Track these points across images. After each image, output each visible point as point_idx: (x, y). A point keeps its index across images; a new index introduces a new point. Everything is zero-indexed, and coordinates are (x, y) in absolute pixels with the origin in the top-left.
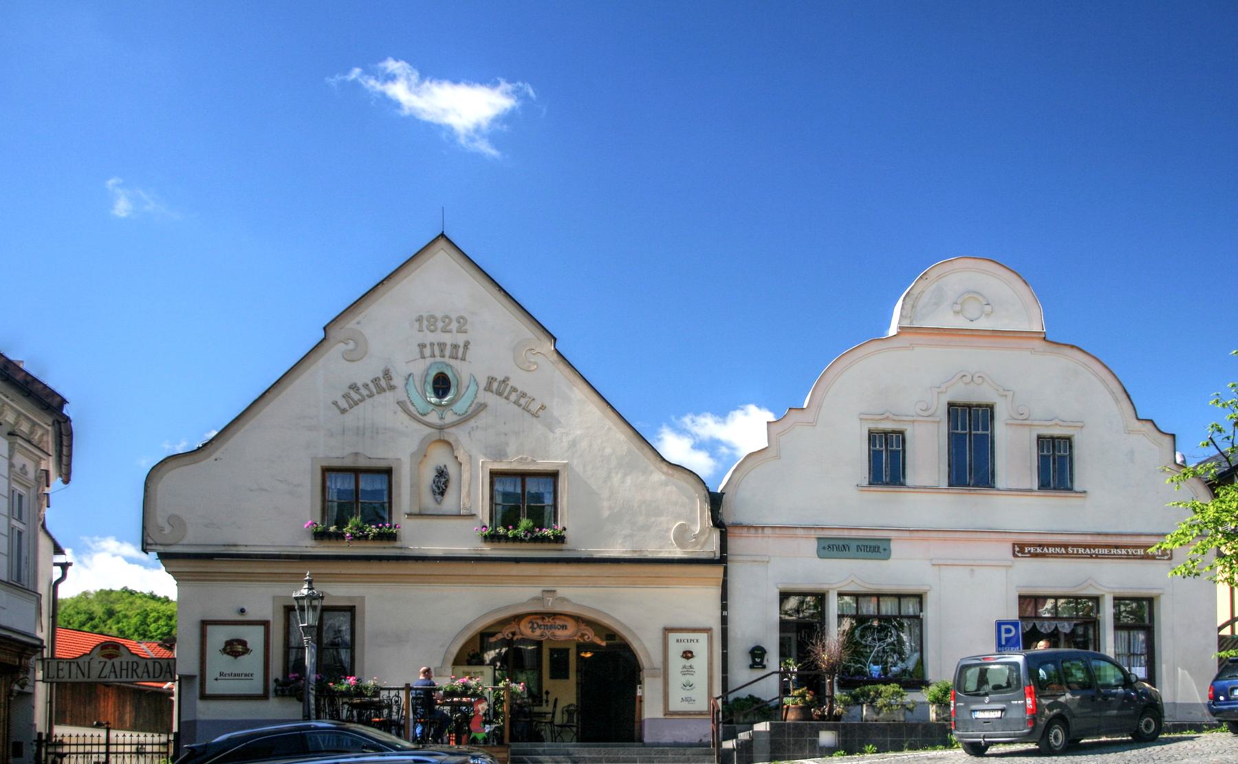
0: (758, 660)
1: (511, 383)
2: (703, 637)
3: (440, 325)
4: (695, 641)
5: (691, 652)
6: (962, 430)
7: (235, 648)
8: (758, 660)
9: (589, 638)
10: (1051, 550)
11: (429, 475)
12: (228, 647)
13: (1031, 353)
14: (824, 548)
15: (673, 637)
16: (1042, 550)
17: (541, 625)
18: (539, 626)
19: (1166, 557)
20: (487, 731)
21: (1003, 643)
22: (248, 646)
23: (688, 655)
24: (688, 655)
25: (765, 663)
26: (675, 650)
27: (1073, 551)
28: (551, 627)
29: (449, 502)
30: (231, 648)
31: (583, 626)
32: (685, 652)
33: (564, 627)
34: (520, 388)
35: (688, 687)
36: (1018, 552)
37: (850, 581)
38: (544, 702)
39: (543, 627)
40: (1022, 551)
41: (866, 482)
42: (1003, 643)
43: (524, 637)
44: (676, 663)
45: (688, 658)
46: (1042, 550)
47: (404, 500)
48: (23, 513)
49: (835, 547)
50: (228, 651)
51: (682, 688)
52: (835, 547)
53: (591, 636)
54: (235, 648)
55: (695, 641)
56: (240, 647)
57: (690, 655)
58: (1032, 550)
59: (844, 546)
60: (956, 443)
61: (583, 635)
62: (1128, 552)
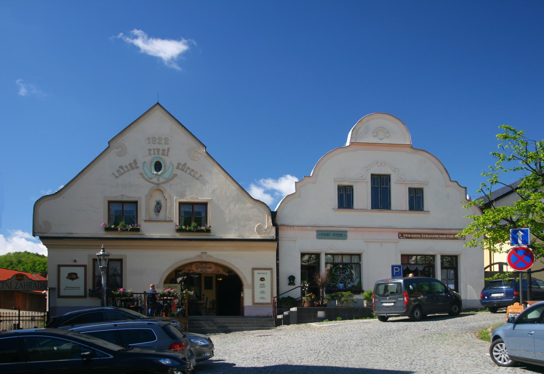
0: (292, 281)
1: (187, 166)
2: (269, 272)
3: (157, 141)
6: (377, 185)
7: (72, 276)
8: (292, 281)
10: (415, 236)
11: (153, 204)
14: (319, 235)
15: (256, 272)
16: (411, 236)
18: (200, 267)
19: (463, 239)
21: (395, 274)
23: (262, 279)
24: (262, 279)
25: (295, 282)
26: (257, 277)
27: (424, 236)
33: (210, 268)
34: (191, 168)
35: (262, 293)
36: (401, 236)
40: (402, 236)
41: (337, 207)
42: (395, 274)
43: (193, 272)
44: (257, 282)
45: (262, 281)
46: (411, 236)
47: (142, 214)
51: (260, 293)
53: (221, 272)
57: (263, 279)
58: (407, 235)
60: (374, 190)
62: (447, 236)
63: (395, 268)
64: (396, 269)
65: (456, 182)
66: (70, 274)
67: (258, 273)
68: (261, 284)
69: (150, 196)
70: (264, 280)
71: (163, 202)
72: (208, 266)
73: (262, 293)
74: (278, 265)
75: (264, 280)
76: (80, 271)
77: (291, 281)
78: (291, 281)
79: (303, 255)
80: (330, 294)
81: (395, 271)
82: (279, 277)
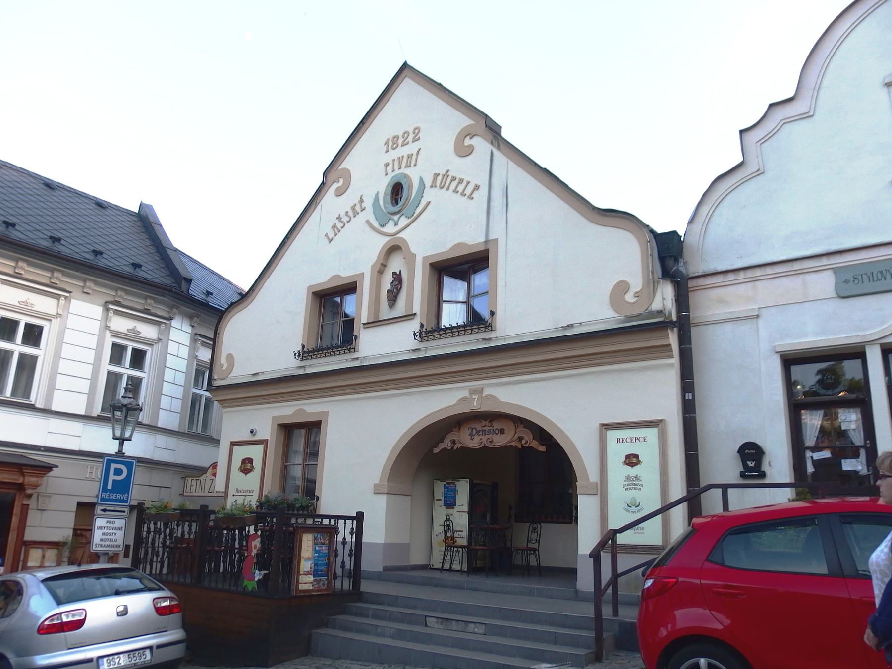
0: (751, 464)
1: (451, 174)
2: (651, 434)
4: (642, 439)
5: (636, 456)
7: (247, 466)
8: (751, 464)
9: (526, 443)
11: (387, 282)
12: (628, 460)
13: (807, 116)
14: (847, 282)
15: (612, 435)
17: (479, 431)
18: (478, 432)
20: (256, 579)
21: (110, 487)
22: (640, 459)
23: (632, 460)
24: (632, 460)
25: (765, 467)
26: (617, 452)
28: (489, 432)
29: (400, 309)
30: (629, 461)
31: (521, 428)
32: (628, 457)
33: (502, 431)
34: (458, 176)
35: (633, 508)
37: (388, 172)
38: (574, 518)
39: (481, 433)
42: (110, 487)
43: (463, 446)
44: (617, 471)
45: (632, 465)
48: (360, 382)
49: (865, 277)
50: (628, 462)
51: (625, 509)
52: (865, 277)
53: (528, 439)
54: (247, 466)
55: (642, 439)
56: (635, 459)
57: (634, 460)
59: (881, 272)
61: (520, 439)
63: (113, 466)
64: (118, 472)
65: (771, 105)
66: (251, 461)
67: (618, 441)
68: (628, 478)
69: (381, 268)
70: (638, 463)
71: (405, 276)
72: (497, 425)
73: (633, 508)
74: (689, 409)
75: (638, 463)
76: (255, 453)
77: (749, 463)
78: (749, 463)
79: (790, 361)
80: (70, 543)
81: (112, 477)
82: (696, 449)
